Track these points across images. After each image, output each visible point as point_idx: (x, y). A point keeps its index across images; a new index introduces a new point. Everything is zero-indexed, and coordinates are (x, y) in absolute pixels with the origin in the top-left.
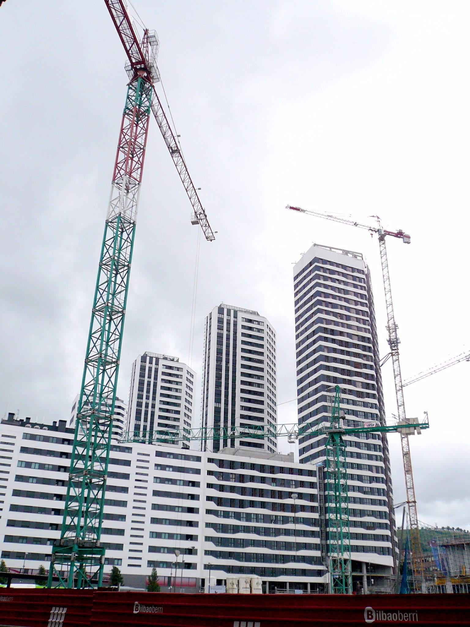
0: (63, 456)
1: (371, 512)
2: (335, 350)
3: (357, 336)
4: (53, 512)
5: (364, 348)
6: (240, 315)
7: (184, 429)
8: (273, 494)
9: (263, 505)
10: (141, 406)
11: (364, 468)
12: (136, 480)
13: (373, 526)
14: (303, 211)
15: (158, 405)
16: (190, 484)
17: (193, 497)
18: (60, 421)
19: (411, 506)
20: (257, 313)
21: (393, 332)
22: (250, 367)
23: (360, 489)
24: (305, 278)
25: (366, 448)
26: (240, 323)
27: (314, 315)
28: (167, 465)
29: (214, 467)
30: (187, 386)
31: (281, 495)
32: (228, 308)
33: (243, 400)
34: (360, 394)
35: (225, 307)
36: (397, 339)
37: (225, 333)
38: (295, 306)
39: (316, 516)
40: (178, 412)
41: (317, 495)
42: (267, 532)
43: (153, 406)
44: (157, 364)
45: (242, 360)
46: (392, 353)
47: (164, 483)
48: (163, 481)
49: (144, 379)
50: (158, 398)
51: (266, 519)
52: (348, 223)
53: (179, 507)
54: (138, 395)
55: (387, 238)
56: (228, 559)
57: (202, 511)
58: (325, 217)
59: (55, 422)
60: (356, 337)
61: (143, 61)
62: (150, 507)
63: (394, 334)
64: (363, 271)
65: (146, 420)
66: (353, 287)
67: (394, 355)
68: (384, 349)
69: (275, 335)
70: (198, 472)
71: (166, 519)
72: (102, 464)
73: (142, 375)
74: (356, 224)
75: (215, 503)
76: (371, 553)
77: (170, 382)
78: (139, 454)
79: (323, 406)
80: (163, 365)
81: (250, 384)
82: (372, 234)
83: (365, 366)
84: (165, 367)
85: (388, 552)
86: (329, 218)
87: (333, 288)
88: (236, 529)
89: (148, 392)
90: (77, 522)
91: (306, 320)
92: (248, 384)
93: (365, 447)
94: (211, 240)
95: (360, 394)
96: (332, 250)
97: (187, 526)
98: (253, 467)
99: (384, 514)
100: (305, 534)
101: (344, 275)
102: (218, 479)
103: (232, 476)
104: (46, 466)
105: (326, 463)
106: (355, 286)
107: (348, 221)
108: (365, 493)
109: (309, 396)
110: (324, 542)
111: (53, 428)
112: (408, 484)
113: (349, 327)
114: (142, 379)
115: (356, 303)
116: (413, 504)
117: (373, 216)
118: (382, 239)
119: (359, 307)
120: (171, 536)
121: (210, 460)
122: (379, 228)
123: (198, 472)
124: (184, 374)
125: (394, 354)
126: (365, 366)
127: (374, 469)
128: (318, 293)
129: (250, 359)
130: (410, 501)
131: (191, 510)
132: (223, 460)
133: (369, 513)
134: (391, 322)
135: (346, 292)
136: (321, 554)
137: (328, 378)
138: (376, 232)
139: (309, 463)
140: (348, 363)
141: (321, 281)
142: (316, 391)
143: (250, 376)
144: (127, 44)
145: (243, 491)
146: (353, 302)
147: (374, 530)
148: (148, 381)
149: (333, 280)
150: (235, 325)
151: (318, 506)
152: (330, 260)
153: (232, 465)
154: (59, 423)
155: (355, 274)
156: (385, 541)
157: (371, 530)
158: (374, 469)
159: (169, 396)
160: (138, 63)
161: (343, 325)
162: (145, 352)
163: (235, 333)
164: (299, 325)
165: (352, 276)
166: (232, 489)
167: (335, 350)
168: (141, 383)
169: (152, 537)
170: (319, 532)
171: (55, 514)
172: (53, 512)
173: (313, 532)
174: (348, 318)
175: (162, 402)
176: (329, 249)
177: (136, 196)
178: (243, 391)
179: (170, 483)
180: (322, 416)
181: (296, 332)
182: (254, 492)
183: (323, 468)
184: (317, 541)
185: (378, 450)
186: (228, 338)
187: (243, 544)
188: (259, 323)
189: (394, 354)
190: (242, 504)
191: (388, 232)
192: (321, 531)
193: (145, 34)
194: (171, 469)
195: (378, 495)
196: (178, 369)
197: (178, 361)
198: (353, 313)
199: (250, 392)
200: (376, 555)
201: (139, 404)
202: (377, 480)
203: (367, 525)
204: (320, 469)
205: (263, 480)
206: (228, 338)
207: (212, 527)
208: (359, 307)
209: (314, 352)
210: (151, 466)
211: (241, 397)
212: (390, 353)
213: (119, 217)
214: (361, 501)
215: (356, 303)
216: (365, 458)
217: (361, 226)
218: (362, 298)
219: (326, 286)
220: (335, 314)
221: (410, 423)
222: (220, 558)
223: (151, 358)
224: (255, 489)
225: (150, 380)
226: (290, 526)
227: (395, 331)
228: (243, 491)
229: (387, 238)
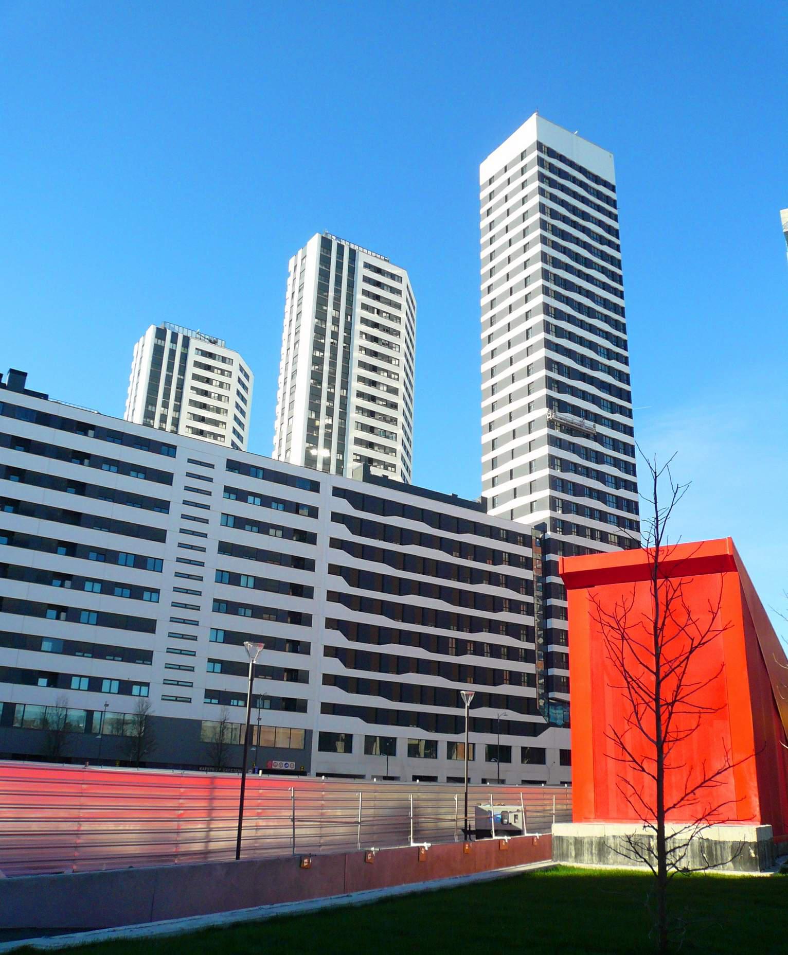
28: (49, 604)
42: (439, 645)
48: (240, 523)
62: (213, 574)
72: (668, 849)
88: (383, 635)
100: (512, 654)
123: (313, 512)
172: (63, 550)
210: (217, 489)
226: (484, 637)
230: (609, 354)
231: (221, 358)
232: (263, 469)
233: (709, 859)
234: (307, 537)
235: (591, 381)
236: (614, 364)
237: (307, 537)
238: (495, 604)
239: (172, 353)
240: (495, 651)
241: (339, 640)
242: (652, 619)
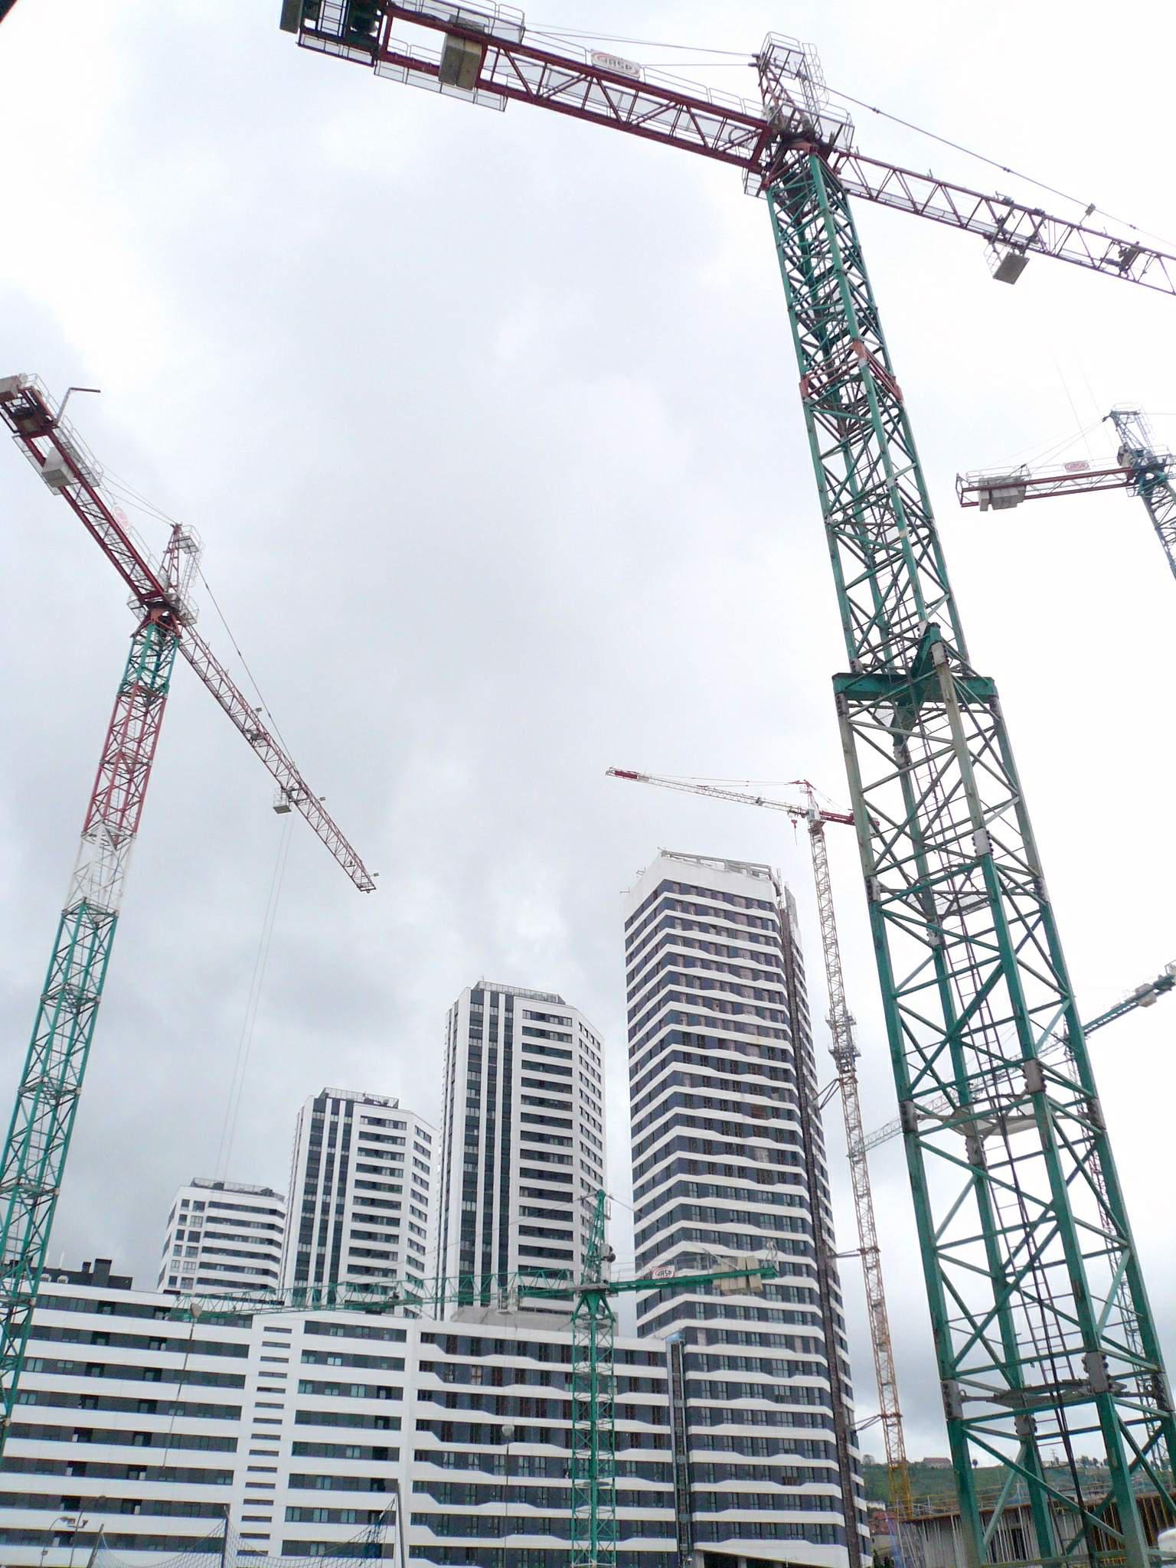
0: (99, 1340)
1: (792, 1443)
2: (707, 1081)
3: (756, 1048)
4: (70, 1470)
5: (773, 1073)
6: (519, 1005)
7: (411, 1260)
8: (566, 1409)
9: (545, 1436)
10: (313, 1211)
11: (775, 1343)
12: (260, 1389)
13: (796, 1476)
14: (645, 779)
15: (350, 1207)
16: (383, 1393)
17: (388, 1423)
18: (98, 1261)
19: (891, 1425)
20: (559, 998)
21: (843, 1032)
22: (542, 1120)
23: (767, 1391)
24: (645, 924)
25: (780, 1297)
26: (520, 1022)
29: (435, 1353)
30: (416, 1162)
31: (584, 1411)
32: (494, 989)
33: (526, 1193)
34: (762, 1176)
35: (488, 988)
36: (852, 1048)
37: (486, 1045)
39: (665, 1456)
40: (395, 1222)
41: (668, 1407)
43: (340, 1209)
44: (349, 1113)
46: (841, 1080)
47: (323, 1393)
49: (318, 1149)
50: (352, 1191)
51: (553, 1467)
52: (742, 800)
53: (354, 1447)
54: (307, 1185)
55: (829, 827)
56: (464, 1564)
57: (407, 1455)
58: (693, 790)
59: (87, 1265)
60: (756, 1050)
61: (157, 591)
62: (296, 1385)
63: (844, 1037)
64: (770, 903)
65: (322, 1242)
66: (748, 939)
67: (846, 1084)
68: (825, 1069)
69: (599, 1044)
70: (398, 1364)
71: (324, 1477)
73: (315, 1141)
74: (759, 802)
75: (436, 1434)
76: (792, 1539)
77: (377, 1153)
78: (267, 1329)
79: (682, 1206)
80: (362, 1117)
81: (542, 1156)
82: (795, 822)
83: (776, 1113)
84: (366, 1120)
85: (834, 1535)
86: (700, 791)
87: (704, 946)
88: (482, 1493)
89: (329, 1177)
90: (1100, 1312)
91: (649, 1016)
92: (536, 1156)
93: (777, 1294)
94: (368, 891)
95: (762, 1176)
96: (702, 861)
97: (371, 1490)
98: (522, 1348)
99: (822, 1447)
100: (640, 1499)
101: (728, 915)
102: (445, 1380)
103: (476, 1372)
104: (60, 1365)
105: (689, 1335)
106: (754, 938)
107: (744, 796)
108: (778, 1399)
109: (654, 1182)
110: (685, 1518)
111: (82, 1278)
112: (884, 1373)
113: (740, 1027)
114: (315, 1148)
115: (756, 974)
116: (894, 1420)
117: (798, 783)
118: (816, 830)
119: (762, 984)
120: (334, 1516)
121: (427, 1338)
122: (811, 808)
124: (410, 1136)
125: (845, 1080)
126: (776, 1113)
127: (798, 1343)
128: (671, 958)
129: (541, 1102)
130: (888, 1413)
131: (381, 1454)
132: (455, 1337)
133: (786, 1447)
134: (839, 1009)
135: (733, 952)
136: (679, 1547)
137: (691, 1144)
138: (803, 815)
139: (652, 1335)
140: (737, 1107)
141: (678, 931)
142: (668, 1173)
143: (541, 1138)
144: (679, 134)
145: (500, 1405)
146: (749, 974)
147: (800, 1484)
148: (328, 1154)
149: (704, 928)
150: (509, 1026)
151: (669, 1432)
152: (695, 885)
153: (476, 1346)
154: (96, 1266)
155: (754, 912)
156: (825, 1510)
157: (795, 1484)
158: (798, 1343)
159: (374, 1186)
160: (151, 594)
161: (725, 1025)
162: (325, 1090)
163: (508, 1045)
164: (634, 1027)
165: (747, 916)
166: (476, 1402)
167: (707, 1081)
168: (314, 1158)
169: (292, 1520)
170: (673, 1493)
171: (74, 1474)
173: (659, 1494)
174: (738, 1009)
175: (360, 1200)
176: (695, 860)
177: (123, 863)
178: (525, 1173)
179: (336, 1392)
180: (678, 1230)
181: (629, 1041)
182: (524, 1406)
183: (683, 1346)
184: (668, 1515)
185: (808, 1300)
186: (493, 1058)
187: (498, 1529)
188: (561, 1020)
189: (845, 1080)
190: (495, 1435)
191: (828, 814)
192: (678, 1490)
193: (175, 533)
194: (338, 1361)
195: (809, 1404)
196: (396, 1125)
197: (396, 1107)
198: (749, 997)
199: (541, 1175)
200: (804, 1543)
201: (309, 1207)
202: (806, 1368)
203: (783, 1475)
204: (675, 1348)
205: (545, 1378)
206: (493, 1058)
207: (428, 1492)
208: (762, 984)
209: (664, 1085)
211: (521, 1187)
212: (836, 1080)
213: (85, 905)
214: (770, 1418)
215: (756, 974)
216: (777, 1320)
217: (770, 805)
218: (769, 963)
219: (688, 942)
220: (708, 1002)
221: (738, 1268)
222: (444, 1564)
223: (336, 1102)
224: (528, 1399)
225: (333, 1151)
227: (848, 1031)
228: (500, 1405)
229: (829, 827)
231: (392, 1123)
234: (392, 1393)
237: (392, 1393)
239: (331, 1159)
241: (428, 1504)
242: (994, 1185)
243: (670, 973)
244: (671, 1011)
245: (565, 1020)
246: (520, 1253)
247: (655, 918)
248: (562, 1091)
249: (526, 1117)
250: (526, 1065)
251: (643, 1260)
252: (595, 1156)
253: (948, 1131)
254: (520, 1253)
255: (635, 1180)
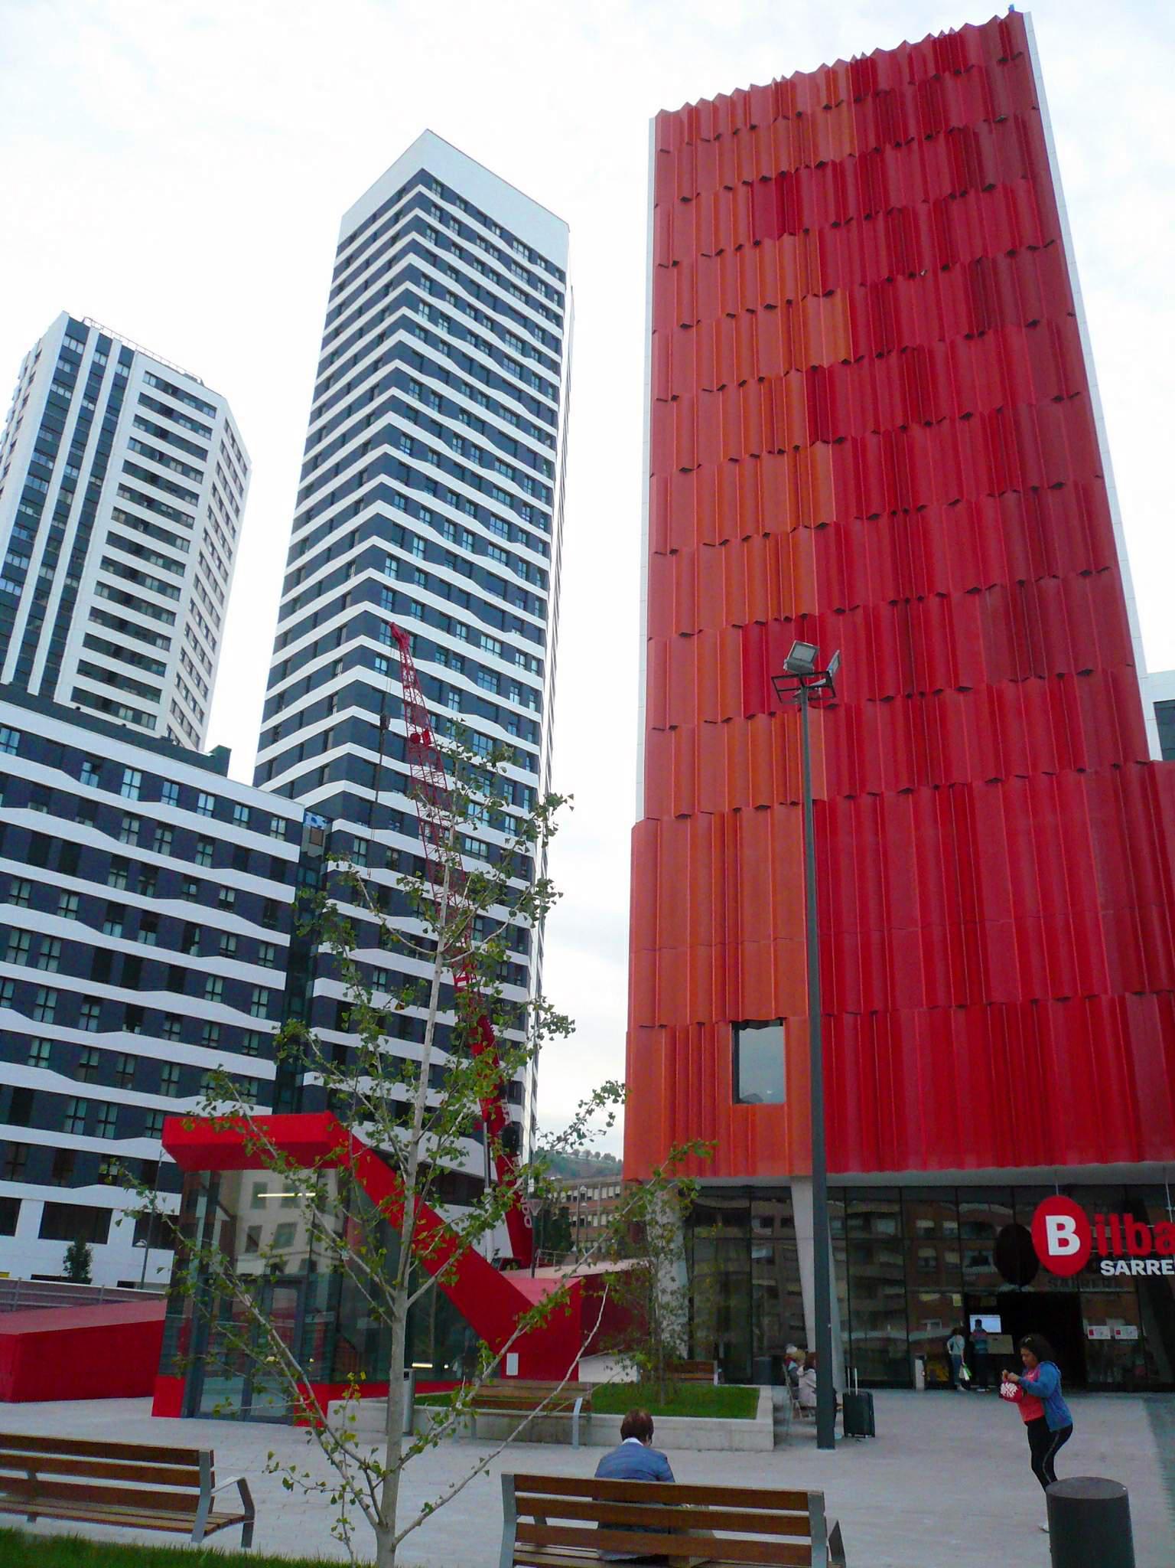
27: (387, 314)
38: (270, 685)
45: (116, 519)
91: (309, 684)
100: (230, 1039)
129: (122, 625)
141: (387, 579)
155: (538, 270)
163: (114, 409)
186: (62, 513)
219: (434, 260)
230: (512, 532)
232: (237, 936)
233: (561, 1173)
235: (469, 570)
236: (519, 549)
238: (208, 941)
240: (192, 1030)
243: (370, 580)
244: (378, 515)
245: (145, 718)
246: (80, 671)
247: (352, 546)
248: (144, 696)
249: (91, 642)
250: (91, 642)
251: (265, 772)
252: (195, 702)
253: (1015, 1406)
254: (80, 671)
255: (267, 716)
